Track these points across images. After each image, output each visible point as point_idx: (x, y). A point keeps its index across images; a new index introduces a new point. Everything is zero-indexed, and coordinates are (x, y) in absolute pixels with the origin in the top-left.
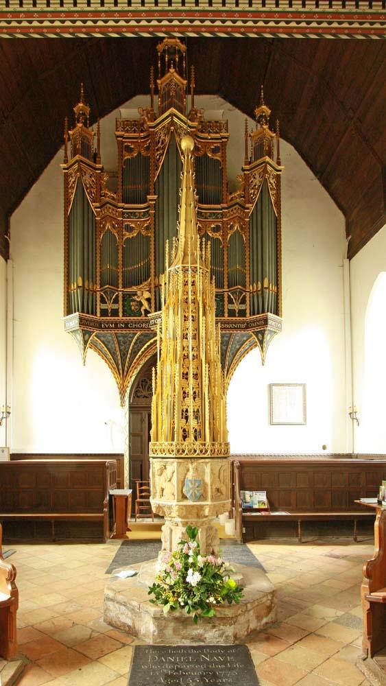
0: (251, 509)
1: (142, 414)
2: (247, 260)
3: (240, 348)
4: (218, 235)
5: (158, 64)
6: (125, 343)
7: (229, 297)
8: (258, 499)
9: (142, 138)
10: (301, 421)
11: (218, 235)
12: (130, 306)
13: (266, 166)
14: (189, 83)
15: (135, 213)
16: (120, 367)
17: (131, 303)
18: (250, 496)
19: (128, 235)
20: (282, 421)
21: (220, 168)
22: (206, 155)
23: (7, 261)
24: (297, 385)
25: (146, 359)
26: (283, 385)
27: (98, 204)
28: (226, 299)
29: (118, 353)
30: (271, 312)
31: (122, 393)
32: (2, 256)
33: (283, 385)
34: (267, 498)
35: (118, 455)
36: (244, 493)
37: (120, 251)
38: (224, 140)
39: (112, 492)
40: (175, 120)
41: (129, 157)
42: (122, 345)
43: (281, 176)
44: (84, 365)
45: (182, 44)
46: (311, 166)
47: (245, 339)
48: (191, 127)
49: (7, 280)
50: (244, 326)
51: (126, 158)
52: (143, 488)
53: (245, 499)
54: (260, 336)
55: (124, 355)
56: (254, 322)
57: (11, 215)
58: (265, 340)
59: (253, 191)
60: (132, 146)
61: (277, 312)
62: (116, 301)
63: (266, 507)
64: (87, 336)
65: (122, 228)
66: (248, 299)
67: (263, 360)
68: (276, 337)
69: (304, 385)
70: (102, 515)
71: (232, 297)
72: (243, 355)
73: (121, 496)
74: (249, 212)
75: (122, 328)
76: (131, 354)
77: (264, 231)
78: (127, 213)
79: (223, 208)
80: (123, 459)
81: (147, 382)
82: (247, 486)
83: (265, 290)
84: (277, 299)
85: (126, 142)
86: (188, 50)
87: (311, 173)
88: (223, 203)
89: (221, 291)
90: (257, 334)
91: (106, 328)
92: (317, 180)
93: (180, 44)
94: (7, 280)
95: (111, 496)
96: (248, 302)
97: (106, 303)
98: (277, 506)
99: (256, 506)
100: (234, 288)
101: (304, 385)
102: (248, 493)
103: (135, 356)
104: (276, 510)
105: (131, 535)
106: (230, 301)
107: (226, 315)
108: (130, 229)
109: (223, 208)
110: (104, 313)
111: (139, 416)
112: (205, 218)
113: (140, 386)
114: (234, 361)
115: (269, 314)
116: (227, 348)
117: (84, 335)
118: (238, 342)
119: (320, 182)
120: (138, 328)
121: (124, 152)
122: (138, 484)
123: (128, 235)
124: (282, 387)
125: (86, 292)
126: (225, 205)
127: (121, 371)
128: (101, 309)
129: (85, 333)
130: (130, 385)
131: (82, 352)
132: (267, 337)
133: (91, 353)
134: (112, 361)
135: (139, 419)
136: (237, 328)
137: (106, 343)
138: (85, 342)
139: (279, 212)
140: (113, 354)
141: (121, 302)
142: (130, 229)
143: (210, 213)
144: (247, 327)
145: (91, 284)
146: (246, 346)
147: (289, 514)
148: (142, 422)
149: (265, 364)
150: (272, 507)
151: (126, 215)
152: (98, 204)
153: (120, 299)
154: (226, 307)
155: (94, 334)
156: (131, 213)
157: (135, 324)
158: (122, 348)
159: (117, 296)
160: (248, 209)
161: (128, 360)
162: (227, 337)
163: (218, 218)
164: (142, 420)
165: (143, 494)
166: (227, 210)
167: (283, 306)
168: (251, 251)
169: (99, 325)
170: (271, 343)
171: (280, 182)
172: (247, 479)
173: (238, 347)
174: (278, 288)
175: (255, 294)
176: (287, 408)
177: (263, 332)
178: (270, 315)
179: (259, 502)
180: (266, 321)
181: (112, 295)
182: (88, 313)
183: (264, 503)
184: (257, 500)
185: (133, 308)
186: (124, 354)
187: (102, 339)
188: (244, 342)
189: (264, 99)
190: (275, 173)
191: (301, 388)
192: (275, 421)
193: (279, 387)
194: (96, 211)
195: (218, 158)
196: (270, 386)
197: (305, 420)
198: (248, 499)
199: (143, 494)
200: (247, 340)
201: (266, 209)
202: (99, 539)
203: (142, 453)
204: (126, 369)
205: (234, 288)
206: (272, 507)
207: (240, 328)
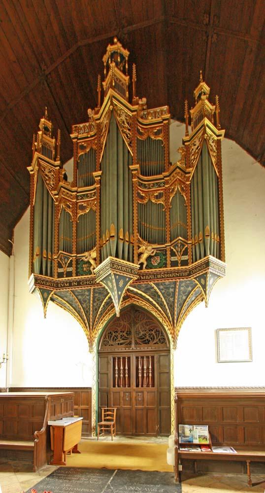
0: (190, 445)
1: (107, 357)
2: (189, 217)
3: (186, 299)
4: (161, 201)
5: (104, 71)
6: (85, 301)
7: (172, 250)
8: (199, 433)
9: (92, 136)
10: (248, 358)
11: (161, 201)
12: (83, 268)
13: (205, 130)
14: (131, 78)
15: (87, 194)
16: (86, 321)
17: (84, 266)
18: (190, 430)
19: (81, 213)
20: (228, 359)
21: (162, 146)
22: (149, 137)
23: (10, 257)
24: (244, 328)
25: (110, 316)
26: (230, 329)
27: (56, 192)
28: (168, 253)
29: (82, 310)
30: (213, 256)
31: (91, 342)
32: (3, 251)
33: (230, 329)
34: (210, 432)
35: (87, 388)
36: (183, 427)
37: (75, 225)
38: (165, 122)
39: (50, 423)
40: (115, 102)
41: (83, 153)
42: (84, 304)
43: (221, 140)
44: (45, 318)
45: (125, 49)
46: (250, 151)
47: (190, 289)
48: (132, 111)
49: (9, 269)
50: (186, 274)
51: (80, 155)
52: (107, 413)
53: (184, 432)
54: (202, 281)
55: (87, 313)
56: (196, 269)
57: (14, 227)
58: (208, 283)
59: (193, 157)
60: (85, 145)
61: (220, 256)
62: (70, 265)
63: (207, 442)
64: (46, 294)
65: (77, 207)
66: (189, 250)
67: (45, 315)
68: (219, 281)
69: (249, 329)
70: (32, 444)
71: (174, 250)
72: (188, 310)
73: (59, 427)
74: (190, 176)
75: (75, 285)
76: (93, 311)
77: (205, 198)
78: (80, 196)
79: (165, 177)
80: (91, 392)
81: (112, 334)
82: (186, 420)
83: (206, 238)
84: (220, 247)
85: (80, 142)
86: (130, 56)
87: (251, 159)
88: (164, 172)
89: (164, 246)
90: (199, 278)
91: (62, 287)
92: (258, 163)
93: (122, 49)
94: (9, 269)
95: (48, 427)
96: (190, 253)
97: (176, 256)
98: (220, 440)
99: (196, 441)
100: (175, 241)
101: (249, 329)
102: (187, 428)
103: (97, 313)
104: (219, 445)
105: (72, 461)
106: (173, 254)
107: (169, 265)
108: (83, 208)
109: (165, 177)
110: (60, 275)
111: (106, 359)
112: (149, 188)
113: (107, 337)
114: (183, 311)
115: (210, 256)
116: (174, 299)
117: (42, 294)
118: (184, 293)
119: (261, 163)
120: (89, 284)
121: (79, 150)
122: (103, 411)
123: (81, 213)
124: (228, 332)
125: (44, 260)
126: (167, 174)
127: (87, 325)
128: (58, 272)
129: (43, 292)
130: (97, 336)
131: (42, 308)
132: (210, 281)
133: (50, 303)
134: (77, 314)
135: (106, 362)
136: (180, 276)
137: (70, 303)
138: (45, 300)
139: (220, 172)
140: (79, 312)
141: (74, 265)
142: (83, 208)
143: (153, 184)
144: (190, 274)
145: (49, 253)
146: (192, 297)
147: (236, 453)
148: (108, 365)
149: (208, 306)
150: (215, 441)
151: (80, 198)
152: (56, 192)
153: (74, 263)
154: (168, 259)
155: (53, 293)
156: (84, 195)
157: (86, 281)
158: (84, 306)
159: (71, 261)
160: (189, 173)
161: (91, 316)
162: (172, 288)
163: (160, 187)
164: (108, 363)
165: (107, 418)
166: (168, 178)
167: (226, 249)
168: (192, 209)
169: (57, 285)
170: (214, 287)
171: (220, 145)
172: (185, 412)
173: (184, 298)
174: (220, 237)
175: (197, 244)
176: (234, 347)
177: (204, 277)
178: (212, 259)
179: (200, 437)
180: (207, 264)
181: (66, 260)
182: (46, 275)
183: (205, 438)
184: (198, 434)
185: (85, 269)
186: (87, 312)
187: (65, 298)
188: (190, 292)
189: (200, 74)
190: (216, 138)
191: (246, 331)
192: (222, 359)
193: (225, 332)
194: (55, 198)
195: (160, 138)
196: (217, 332)
197: (251, 357)
198: (187, 432)
199: (107, 418)
200: (192, 290)
201: (206, 171)
202: (30, 469)
203: (108, 387)
204: (91, 324)
205: (175, 241)
206: (215, 441)
207: (182, 276)
